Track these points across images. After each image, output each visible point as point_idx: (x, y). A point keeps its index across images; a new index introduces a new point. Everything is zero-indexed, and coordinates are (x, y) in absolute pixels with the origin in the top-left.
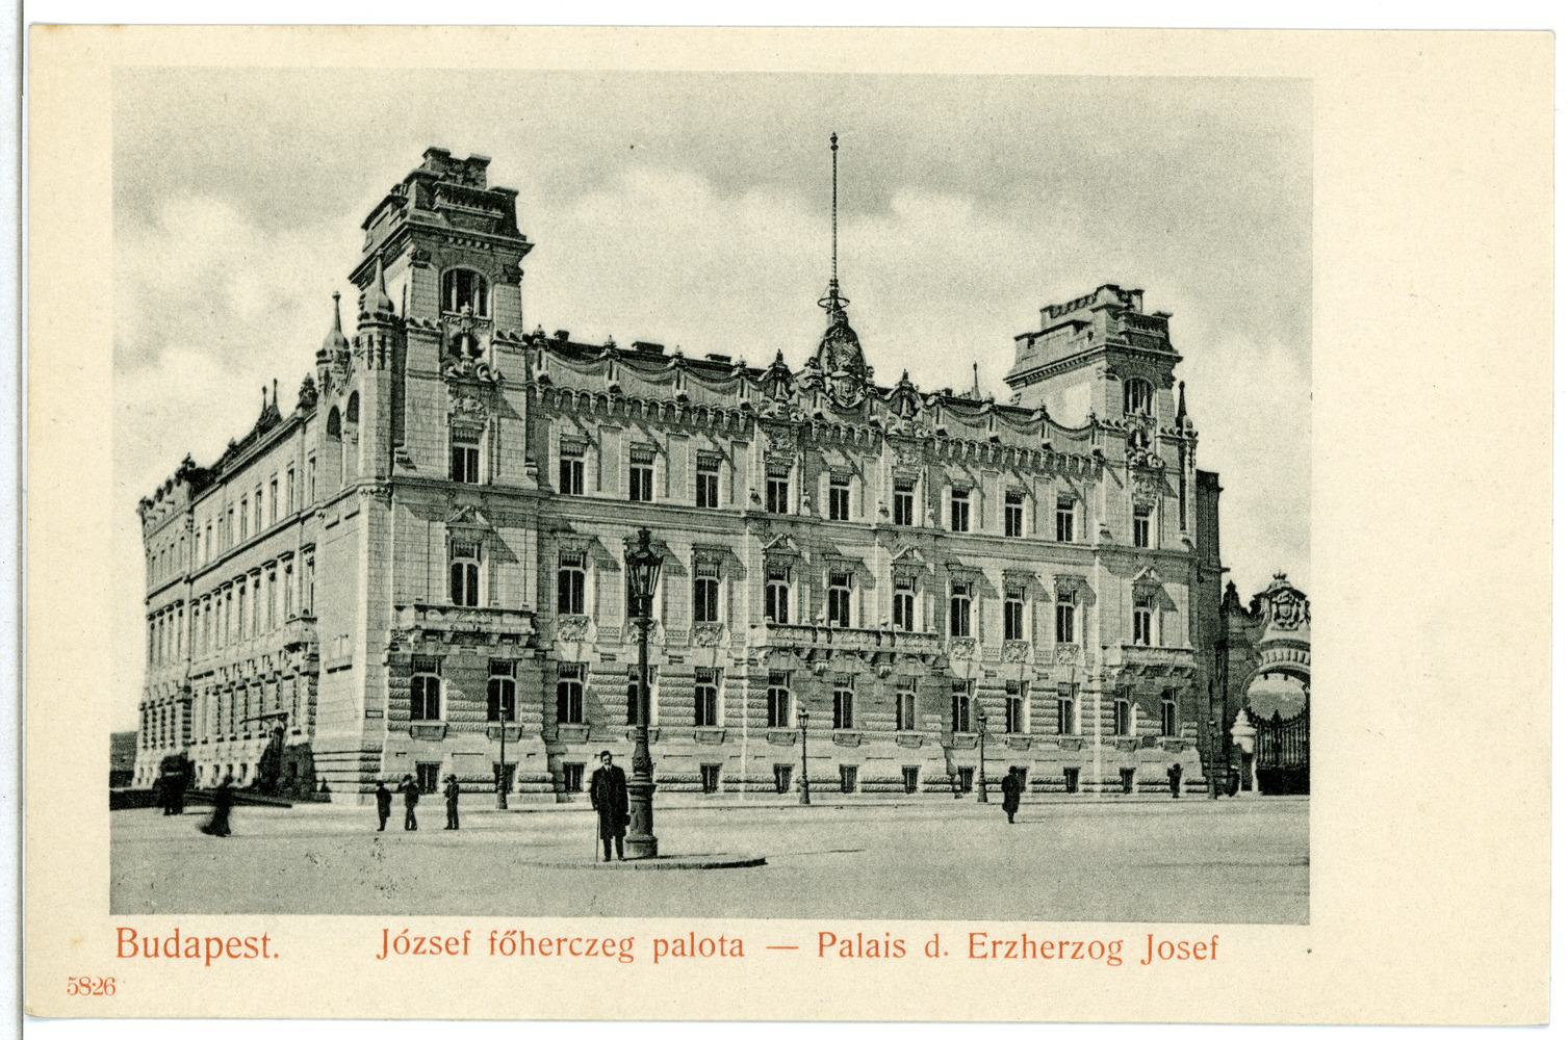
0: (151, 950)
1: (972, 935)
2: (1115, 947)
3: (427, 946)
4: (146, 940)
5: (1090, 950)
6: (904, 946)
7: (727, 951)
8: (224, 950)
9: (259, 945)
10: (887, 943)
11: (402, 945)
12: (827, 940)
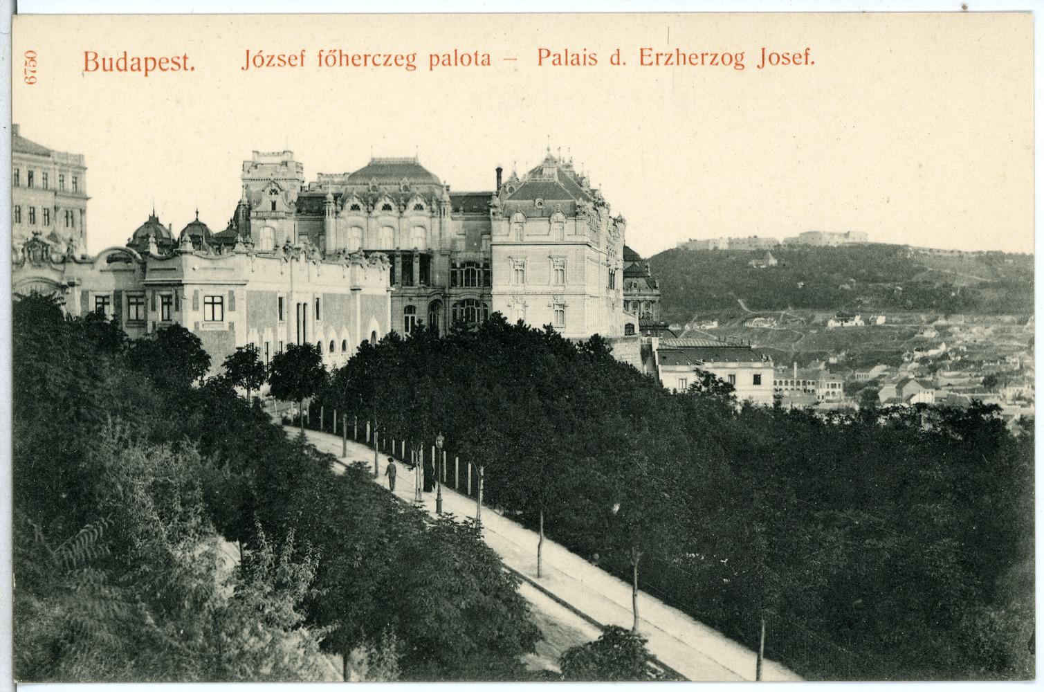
0: (108, 66)
1: (642, 50)
2: (739, 57)
3: (275, 61)
4: (104, 59)
5: (263, 61)
6: (596, 58)
7: (479, 62)
8: (157, 65)
9: (181, 62)
10: (585, 55)
11: (258, 61)
12: (544, 53)
